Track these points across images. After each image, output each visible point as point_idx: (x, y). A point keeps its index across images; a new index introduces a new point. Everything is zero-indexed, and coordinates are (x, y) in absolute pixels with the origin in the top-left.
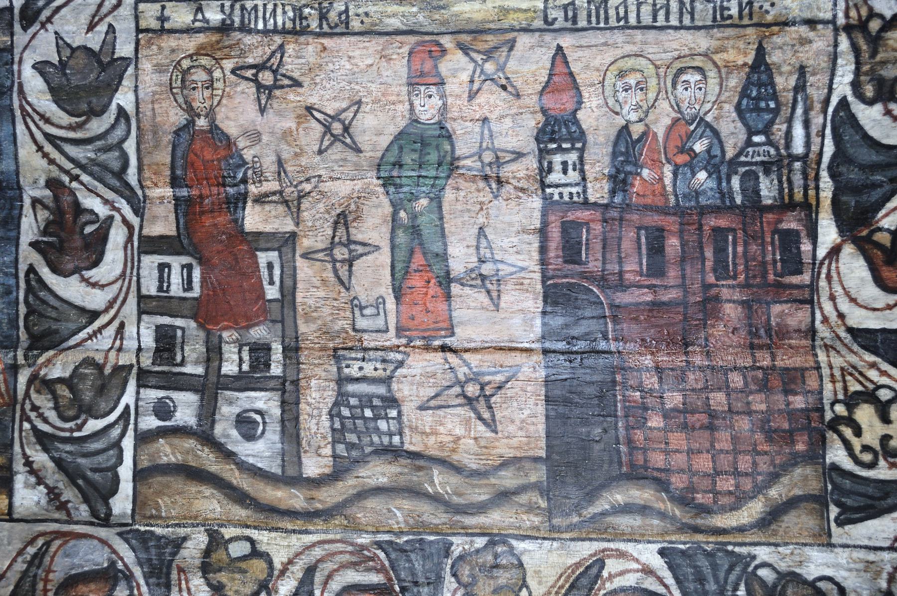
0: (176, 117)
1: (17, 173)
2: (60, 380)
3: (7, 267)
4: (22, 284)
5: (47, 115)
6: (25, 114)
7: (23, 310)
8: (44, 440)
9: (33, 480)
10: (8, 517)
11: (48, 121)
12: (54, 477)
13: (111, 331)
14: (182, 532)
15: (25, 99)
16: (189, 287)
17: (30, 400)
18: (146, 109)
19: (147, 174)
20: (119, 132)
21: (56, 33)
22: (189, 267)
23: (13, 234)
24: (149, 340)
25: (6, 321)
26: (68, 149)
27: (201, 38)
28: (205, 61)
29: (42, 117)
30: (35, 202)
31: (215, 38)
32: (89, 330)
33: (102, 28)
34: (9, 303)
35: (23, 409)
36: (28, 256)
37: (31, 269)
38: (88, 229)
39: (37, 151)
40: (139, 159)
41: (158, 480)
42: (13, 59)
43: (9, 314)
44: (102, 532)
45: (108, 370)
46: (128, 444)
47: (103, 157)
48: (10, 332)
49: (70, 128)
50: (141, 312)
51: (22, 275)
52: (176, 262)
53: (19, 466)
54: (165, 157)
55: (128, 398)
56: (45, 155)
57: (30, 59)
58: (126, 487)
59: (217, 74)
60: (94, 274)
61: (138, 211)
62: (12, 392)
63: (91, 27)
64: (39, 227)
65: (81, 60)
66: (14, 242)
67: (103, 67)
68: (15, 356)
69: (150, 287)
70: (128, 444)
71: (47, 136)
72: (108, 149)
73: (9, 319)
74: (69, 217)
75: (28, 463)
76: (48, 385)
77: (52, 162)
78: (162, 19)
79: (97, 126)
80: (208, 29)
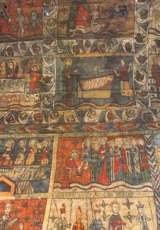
0: (152, 63)
2: (140, 93)
4: (134, 82)
6: (135, 63)
7: (134, 85)
8: (139, 99)
9: (138, 104)
11: (137, 64)
12: (141, 103)
13: (145, 87)
14: (157, 108)
16: (154, 82)
18: (149, 62)
19: (148, 70)
20: (146, 65)
22: (154, 80)
23: (132, 77)
24: (150, 88)
26: (140, 67)
27: (156, 55)
28: (156, 57)
30: (134, 73)
31: (157, 55)
32: (142, 87)
33: (144, 54)
36: (134, 79)
37: (135, 81)
38: (141, 76)
40: (148, 68)
41: (153, 103)
44: (147, 109)
45: (146, 91)
46: (150, 99)
47: (144, 68)
49: (140, 65)
50: (148, 85)
51: (134, 81)
52: (152, 79)
53: (137, 102)
54: (151, 68)
55: (149, 94)
57: (136, 57)
58: (150, 104)
59: (158, 59)
60: (142, 81)
61: (147, 74)
63: (143, 54)
65: (142, 57)
67: (144, 58)
69: (149, 82)
70: (150, 99)
71: (137, 66)
72: (144, 67)
74: (139, 75)
75: (138, 102)
76: (139, 93)
77: (137, 68)
78: (151, 53)
79: (143, 64)
80: (156, 54)
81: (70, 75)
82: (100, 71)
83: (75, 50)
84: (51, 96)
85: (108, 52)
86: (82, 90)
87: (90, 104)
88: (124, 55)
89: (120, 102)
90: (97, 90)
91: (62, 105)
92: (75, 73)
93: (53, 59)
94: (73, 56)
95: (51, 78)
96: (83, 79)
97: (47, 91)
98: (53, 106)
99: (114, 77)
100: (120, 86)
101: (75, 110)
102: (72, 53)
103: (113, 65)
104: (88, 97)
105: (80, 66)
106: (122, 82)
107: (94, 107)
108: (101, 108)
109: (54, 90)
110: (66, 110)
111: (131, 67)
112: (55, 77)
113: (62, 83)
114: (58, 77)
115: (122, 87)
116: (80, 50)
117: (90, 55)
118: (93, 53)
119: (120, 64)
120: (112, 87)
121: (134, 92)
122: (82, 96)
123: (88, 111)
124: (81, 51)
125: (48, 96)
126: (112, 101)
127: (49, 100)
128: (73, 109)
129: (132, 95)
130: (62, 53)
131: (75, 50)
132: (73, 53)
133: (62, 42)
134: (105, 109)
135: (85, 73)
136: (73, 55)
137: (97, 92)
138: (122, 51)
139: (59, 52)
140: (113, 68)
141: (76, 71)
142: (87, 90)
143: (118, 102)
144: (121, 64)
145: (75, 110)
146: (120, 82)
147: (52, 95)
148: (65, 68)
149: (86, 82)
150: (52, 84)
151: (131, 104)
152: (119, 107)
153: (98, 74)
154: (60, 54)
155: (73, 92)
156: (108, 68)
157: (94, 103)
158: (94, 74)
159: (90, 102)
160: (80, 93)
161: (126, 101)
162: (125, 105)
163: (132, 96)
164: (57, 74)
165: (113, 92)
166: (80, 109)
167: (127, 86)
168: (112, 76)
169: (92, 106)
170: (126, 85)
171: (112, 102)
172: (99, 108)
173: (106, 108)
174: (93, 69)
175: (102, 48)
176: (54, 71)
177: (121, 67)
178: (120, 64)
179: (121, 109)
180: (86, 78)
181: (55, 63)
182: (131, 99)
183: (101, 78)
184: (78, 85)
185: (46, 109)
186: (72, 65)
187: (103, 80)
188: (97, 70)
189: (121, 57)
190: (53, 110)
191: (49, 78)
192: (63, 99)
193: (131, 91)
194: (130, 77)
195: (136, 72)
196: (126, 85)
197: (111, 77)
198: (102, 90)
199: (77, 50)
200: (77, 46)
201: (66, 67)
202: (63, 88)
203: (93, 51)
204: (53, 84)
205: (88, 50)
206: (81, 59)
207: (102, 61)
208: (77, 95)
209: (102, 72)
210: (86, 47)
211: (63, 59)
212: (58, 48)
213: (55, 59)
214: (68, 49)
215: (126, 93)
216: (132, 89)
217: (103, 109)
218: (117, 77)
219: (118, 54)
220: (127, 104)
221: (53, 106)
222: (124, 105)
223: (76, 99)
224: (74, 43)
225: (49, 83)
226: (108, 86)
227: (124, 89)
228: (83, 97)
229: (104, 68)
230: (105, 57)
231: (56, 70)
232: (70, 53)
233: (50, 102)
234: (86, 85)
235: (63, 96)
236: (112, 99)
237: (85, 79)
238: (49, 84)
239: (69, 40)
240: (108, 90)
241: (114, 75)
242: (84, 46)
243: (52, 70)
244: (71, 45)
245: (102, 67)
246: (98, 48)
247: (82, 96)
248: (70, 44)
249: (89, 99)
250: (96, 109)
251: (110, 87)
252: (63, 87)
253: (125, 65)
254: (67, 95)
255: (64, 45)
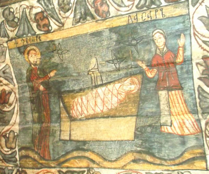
1: (191, 55)
3: (190, 87)
5: (203, 35)
7: (198, 100)
10: (206, 169)
11: (204, 36)
15: (196, 30)
17: (207, 130)
21: (206, 6)
23: (191, 76)
25: (192, 105)
29: (202, 35)
30: (197, 64)
34: (193, 99)
35: (206, 134)
36: (198, 83)
37: (199, 87)
39: (199, 47)
42: (190, 17)
43: (193, 103)
48: (194, 109)
56: (202, 48)
62: (200, 128)
64: (200, 73)
66: (192, 78)
68: (198, 116)
73: (193, 104)
77: (205, 50)
81: (42, 83)
82: (104, 69)
83: (42, 23)
84: (11, 135)
85: (116, 16)
86: (72, 119)
87: (87, 154)
88: (159, 16)
89: (160, 151)
90: (103, 117)
91: (32, 157)
92: (52, 80)
93: (4, 53)
94: (40, 40)
95: (10, 93)
96: (69, 92)
97: (5, 122)
98: (17, 157)
99: (140, 80)
100: (158, 106)
101: (58, 169)
102: (36, 33)
103: (133, 49)
104: (82, 139)
105: (58, 62)
106: (163, 94)
107: (98, 164)
108: (113, 166)
109: (18, 121)
110: (41, 168)
111: (184, 48)
112: (17, 91)
113: (29, 104)
114: (21, 91)
115: (163, 106)
116: (52, 24)
117: (74, 32)
118: (80, 24)
119: (152, 42)
120: (139, 108)
121: (199, 121)
122: (70, 135)
123: (84, 171)
124: (54, 25)
125: (8, 135)
126: (139, 149)
127: (9, 146)
128: (53, 165)
129: (192, 131)
130: (18, 37)
131: (42, 23)
132: (38, 32)
133: (10, 12)
134: (122, 168)
135: (72, 76)
136: (38, 36)
137: (103, 124)
138: (153, 6)
139: (11, 35)
140: (135, 57)
141: (52, 74)
142: (80, 120)
143: (154, 151)
144: (155, 44)
145: (58, 169)
146: (157, 93)
147: (14, 133)
148: (30, 71)
149: (76, 100)
150: (12, 107)
151: (191, 156)
152: (159, 165)
153: (101, 76)
154: (15, 38)
155: (53, 125)
156: (122, 59)
157: (98, 154)
158: (92, 78)
159: (87, 150)
160: (66, 125)
161: (176, 150)
162: (173, 160)
163: (194, 134)
164: (20, 85)
165: (142, 124)
166: (68, 167)
167: (177, 105)
168: (135, 80)
169: (93, 162)
170: (176, 101)
171: (139, 152)
172: (109, 166)
173: (125, 166)
174: (87, 65)
175: (99, 7)
176: (12, 79)
177: (156, 51)
178: (152, 42)
179: (166, 170)
180: (76, 88)
181: (9, 61)
182: (192, 143)
183: (110, 87)
184: (60, 108)
185: (6, 163)
186: (41, 62)
187: (115, 92)
188: (96, 67)
189: (154, 23)
190: (16, 166)
191: (7, 95)
192: (33, 142)
193: (189, 119)
194: (186, 76)
195: (201, 61)
196: (176, 101)
197: (132, 83)
198: (114, 116)
199: (44, 23)
200: (42, 12)
201: (31, 68)
202: (33, 117)
203: (80, 18)
204: (14, 108)
205: (68, 20)
206: (57, 43)
207: (105, 43)
208: (59, 133)
209: (110, 71)
210: (61, 12)
211: (22, 50)
212: (7, 26)
213: (8, 51)
214: (26, 26)
215: (175, 123)
216: (194, 112)
217: (119, 168)
218: (150, 80)
219: (142, 17)
220: (178, 157)
221: (17, 157)
222: (170, 160)
223: (57, 142)
224: (34, 7)
225: (7, 106)
226: (127, 106)
227: (171, 114)
228: (73, 138)
229: (113, 61)
230: (112, 30)
231: (15, 76)
232: (33, 32)
233: (11, 148)
234: (77, 105)
235: (32, 135)
236: (140, 142)
237: (73, 91)
238: (7, 108)
239: (23, 3)
240: (129, 118)
241: (140, 77)
242: (57, 11)
243: (7, 76)
244: (30, 12)
245: (107, 59)
246: (89, 9)
247: (70, 135)
248: (27, 11)
249: (84, 142)
250: (102, 167)
251: (134, 110)
252: (32, 113)
253: (165, 44)
254: (40, 132)
255: (16, 16)
